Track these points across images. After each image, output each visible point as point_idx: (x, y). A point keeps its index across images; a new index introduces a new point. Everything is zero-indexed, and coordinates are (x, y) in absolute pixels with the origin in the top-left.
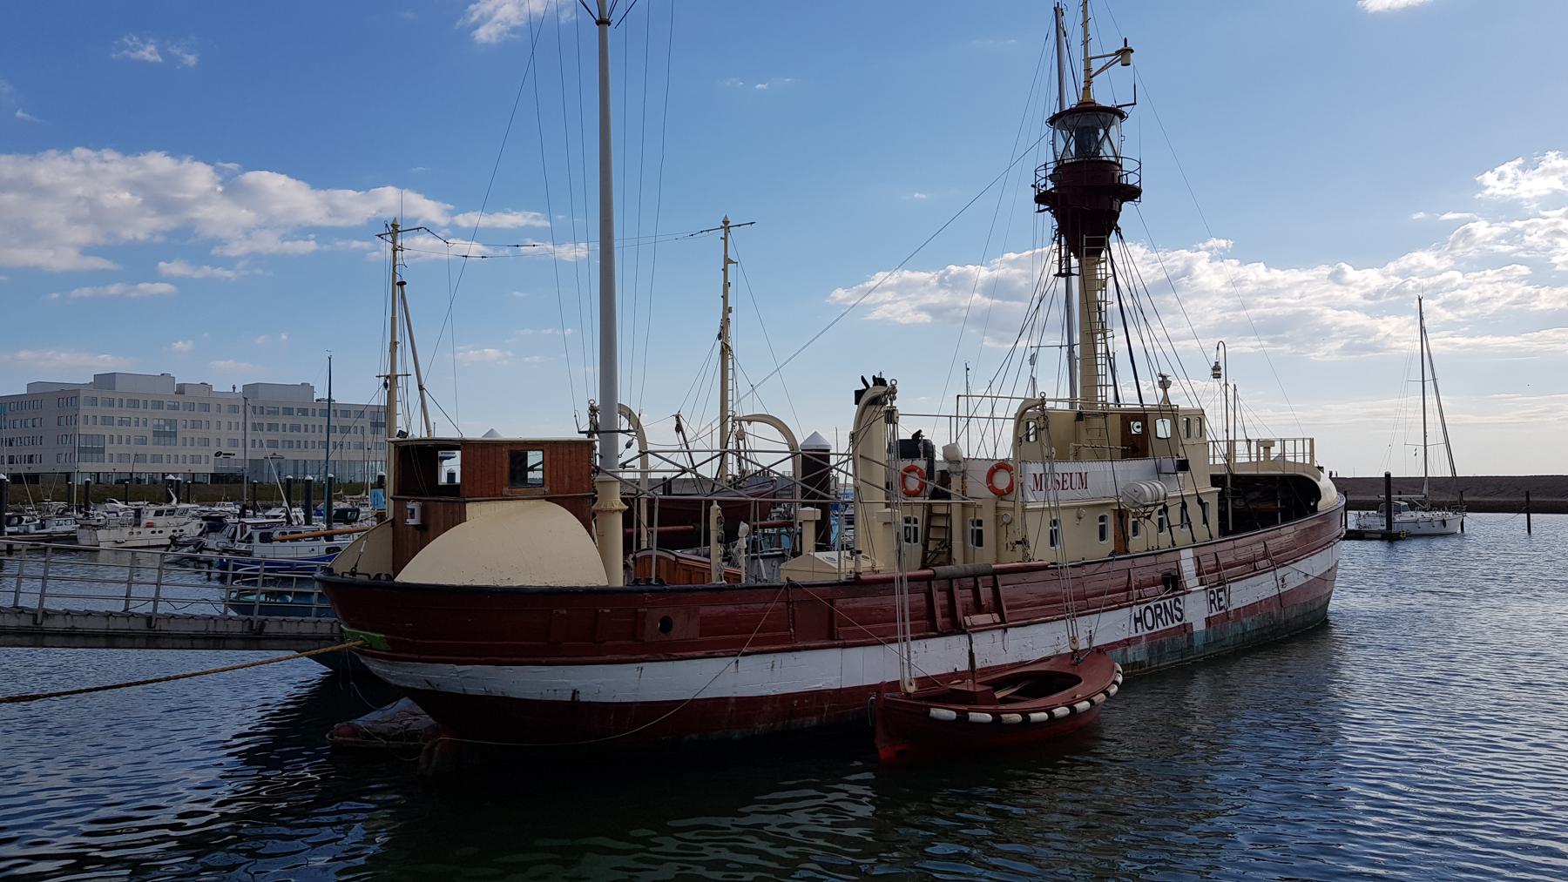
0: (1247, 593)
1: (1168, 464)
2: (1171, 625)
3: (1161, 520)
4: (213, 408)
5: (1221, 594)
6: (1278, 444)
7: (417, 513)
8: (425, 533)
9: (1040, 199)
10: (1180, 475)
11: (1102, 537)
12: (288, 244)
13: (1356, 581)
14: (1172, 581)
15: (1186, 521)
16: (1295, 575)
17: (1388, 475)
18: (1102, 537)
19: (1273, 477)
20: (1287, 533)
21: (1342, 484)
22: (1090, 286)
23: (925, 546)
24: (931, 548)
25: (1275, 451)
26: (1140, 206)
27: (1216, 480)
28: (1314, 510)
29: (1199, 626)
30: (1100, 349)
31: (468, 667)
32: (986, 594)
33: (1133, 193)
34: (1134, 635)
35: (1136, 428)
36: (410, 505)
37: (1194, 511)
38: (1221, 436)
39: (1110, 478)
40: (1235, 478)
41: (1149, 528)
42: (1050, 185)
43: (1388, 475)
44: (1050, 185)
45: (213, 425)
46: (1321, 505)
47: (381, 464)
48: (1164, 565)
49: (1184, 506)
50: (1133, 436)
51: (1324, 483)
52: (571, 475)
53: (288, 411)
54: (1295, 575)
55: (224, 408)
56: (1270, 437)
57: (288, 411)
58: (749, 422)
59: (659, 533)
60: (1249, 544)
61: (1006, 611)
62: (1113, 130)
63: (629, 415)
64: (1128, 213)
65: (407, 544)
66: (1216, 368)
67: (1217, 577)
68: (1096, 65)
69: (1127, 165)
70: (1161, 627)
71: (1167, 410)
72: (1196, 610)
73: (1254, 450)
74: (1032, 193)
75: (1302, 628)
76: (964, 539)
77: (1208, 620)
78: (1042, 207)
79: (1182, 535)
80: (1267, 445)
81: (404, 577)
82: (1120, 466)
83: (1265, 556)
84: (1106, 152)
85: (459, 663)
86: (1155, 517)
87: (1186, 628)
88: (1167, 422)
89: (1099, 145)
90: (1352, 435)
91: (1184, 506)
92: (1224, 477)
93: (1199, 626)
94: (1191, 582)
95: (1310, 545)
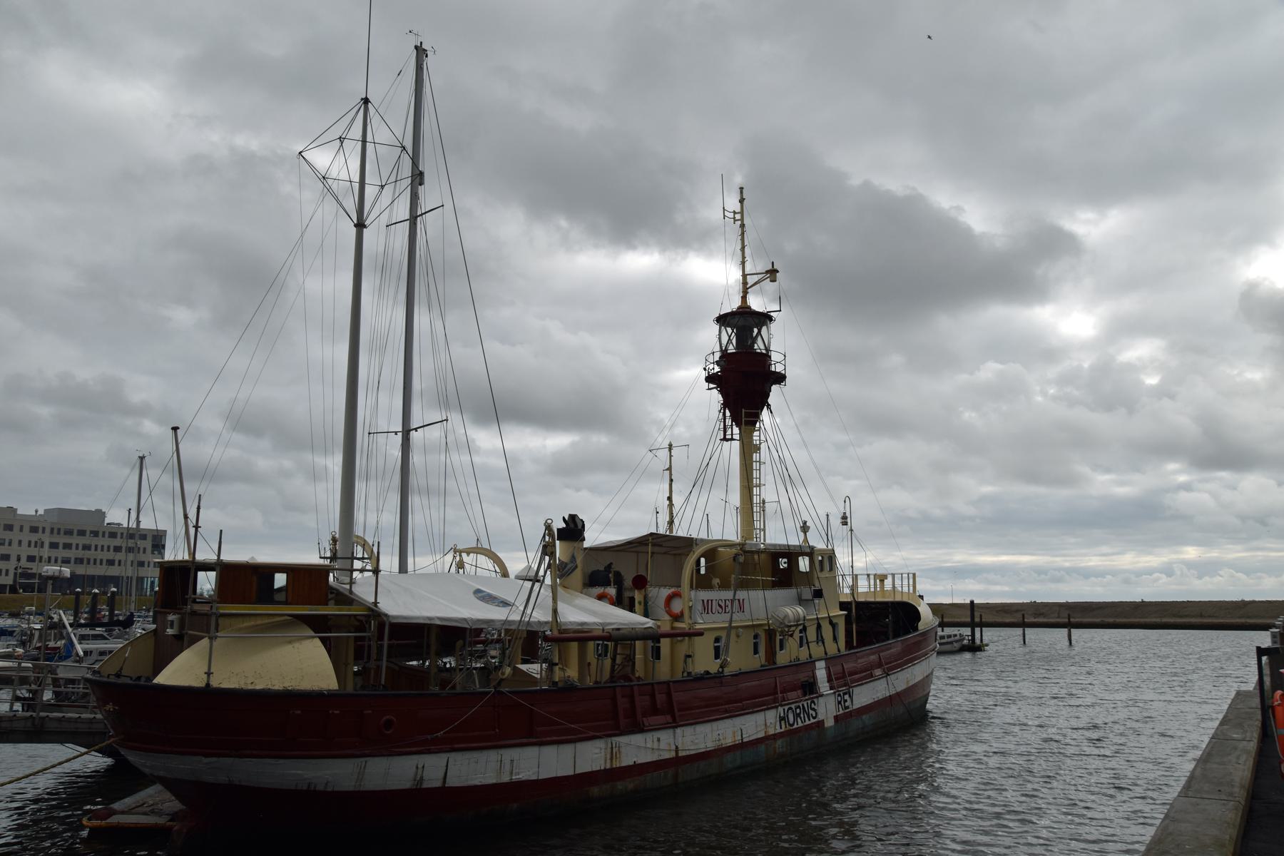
0: (864, 696)
1: (807, 593)
2: (808, 722)
3: (801, 638)
4: (16, 528)
5: (847, 697)
6: (890, 578)
7: (176, 625)
8: (181, 643)
9: (710, 379)
10: (816, 601)
11: (756, 652)
12: (1207, 579)
13: (948, 686)
14: (810, 688)
15: (820, 639)
16: (901, 680)
17: (972, 602)
18: (756, 652)
19: (886, 603)
20: (895, 646)
21: (935, 608)
22: (748, 451)
23: (614, 660)
24: (618, 660)
25: (888, 584)
26: (785, 389)
27: (843, 606)
28: (916, 629)
29: (830, 723)
30: (756, 499)
31: (214, 759)
32: (661, 698)
33: (780, 378)
34: (779, 730)
35: (783, 563)
36: (171, 617)
37: (827, 631)
38: (847, 571)
39: (762, 603)
40: (859, 604)
41: (792, 643)
42: (717, 369)
43: (972, 602)
44: (717, 369)
45: (15, 543)
46: (922, 626)
47: (152, 576)
48: (803, 676)
49: (819, 627)
50: (781, 568)
51: (924, 610)
52: (309, 597)
53: (82, 533)
54: (901, 680)
55: (26, 529)
56: (884, 572)
57: (82, 533)
58: (468, 554)
59: (390, 646)
60: (868, 655)
61: (677, 714)
62: (764, 329)
63: (364, 545)
64: (776, 394)
65: (164, 651)
66: (844, 517)
67: (843, 680)
68: (751, 280)
69: (775, 357)
70: (800, 724)
71: (811, 553)
72: (826, 709)
73: (872, 582)
74: (704, 374)
75: (907, 721)
76: (645, 654)
77: (836, 718)
78: (712, 386)
79: (817, 650)
80: (882, 578)
81: (161, 679)
82: (770, 594)
83: (880, 665)
84: (759, 346)
85: (206, 756)
86: (797, 635)
87: (820, 724)
88: (807, 559)
89: (754, 340)
90: (940, 572)
91: (819, 627)
92: (850, 603)
93: (830, 723)
94: (824, 686)
95: (912, 654)
